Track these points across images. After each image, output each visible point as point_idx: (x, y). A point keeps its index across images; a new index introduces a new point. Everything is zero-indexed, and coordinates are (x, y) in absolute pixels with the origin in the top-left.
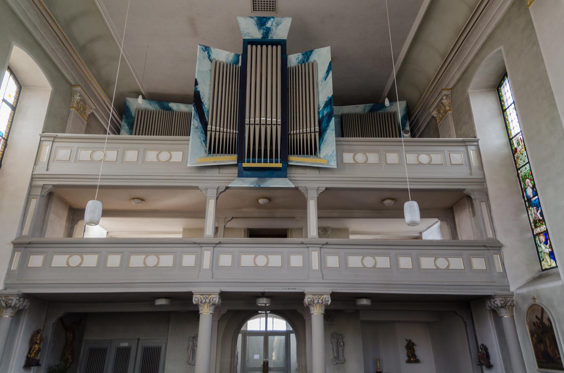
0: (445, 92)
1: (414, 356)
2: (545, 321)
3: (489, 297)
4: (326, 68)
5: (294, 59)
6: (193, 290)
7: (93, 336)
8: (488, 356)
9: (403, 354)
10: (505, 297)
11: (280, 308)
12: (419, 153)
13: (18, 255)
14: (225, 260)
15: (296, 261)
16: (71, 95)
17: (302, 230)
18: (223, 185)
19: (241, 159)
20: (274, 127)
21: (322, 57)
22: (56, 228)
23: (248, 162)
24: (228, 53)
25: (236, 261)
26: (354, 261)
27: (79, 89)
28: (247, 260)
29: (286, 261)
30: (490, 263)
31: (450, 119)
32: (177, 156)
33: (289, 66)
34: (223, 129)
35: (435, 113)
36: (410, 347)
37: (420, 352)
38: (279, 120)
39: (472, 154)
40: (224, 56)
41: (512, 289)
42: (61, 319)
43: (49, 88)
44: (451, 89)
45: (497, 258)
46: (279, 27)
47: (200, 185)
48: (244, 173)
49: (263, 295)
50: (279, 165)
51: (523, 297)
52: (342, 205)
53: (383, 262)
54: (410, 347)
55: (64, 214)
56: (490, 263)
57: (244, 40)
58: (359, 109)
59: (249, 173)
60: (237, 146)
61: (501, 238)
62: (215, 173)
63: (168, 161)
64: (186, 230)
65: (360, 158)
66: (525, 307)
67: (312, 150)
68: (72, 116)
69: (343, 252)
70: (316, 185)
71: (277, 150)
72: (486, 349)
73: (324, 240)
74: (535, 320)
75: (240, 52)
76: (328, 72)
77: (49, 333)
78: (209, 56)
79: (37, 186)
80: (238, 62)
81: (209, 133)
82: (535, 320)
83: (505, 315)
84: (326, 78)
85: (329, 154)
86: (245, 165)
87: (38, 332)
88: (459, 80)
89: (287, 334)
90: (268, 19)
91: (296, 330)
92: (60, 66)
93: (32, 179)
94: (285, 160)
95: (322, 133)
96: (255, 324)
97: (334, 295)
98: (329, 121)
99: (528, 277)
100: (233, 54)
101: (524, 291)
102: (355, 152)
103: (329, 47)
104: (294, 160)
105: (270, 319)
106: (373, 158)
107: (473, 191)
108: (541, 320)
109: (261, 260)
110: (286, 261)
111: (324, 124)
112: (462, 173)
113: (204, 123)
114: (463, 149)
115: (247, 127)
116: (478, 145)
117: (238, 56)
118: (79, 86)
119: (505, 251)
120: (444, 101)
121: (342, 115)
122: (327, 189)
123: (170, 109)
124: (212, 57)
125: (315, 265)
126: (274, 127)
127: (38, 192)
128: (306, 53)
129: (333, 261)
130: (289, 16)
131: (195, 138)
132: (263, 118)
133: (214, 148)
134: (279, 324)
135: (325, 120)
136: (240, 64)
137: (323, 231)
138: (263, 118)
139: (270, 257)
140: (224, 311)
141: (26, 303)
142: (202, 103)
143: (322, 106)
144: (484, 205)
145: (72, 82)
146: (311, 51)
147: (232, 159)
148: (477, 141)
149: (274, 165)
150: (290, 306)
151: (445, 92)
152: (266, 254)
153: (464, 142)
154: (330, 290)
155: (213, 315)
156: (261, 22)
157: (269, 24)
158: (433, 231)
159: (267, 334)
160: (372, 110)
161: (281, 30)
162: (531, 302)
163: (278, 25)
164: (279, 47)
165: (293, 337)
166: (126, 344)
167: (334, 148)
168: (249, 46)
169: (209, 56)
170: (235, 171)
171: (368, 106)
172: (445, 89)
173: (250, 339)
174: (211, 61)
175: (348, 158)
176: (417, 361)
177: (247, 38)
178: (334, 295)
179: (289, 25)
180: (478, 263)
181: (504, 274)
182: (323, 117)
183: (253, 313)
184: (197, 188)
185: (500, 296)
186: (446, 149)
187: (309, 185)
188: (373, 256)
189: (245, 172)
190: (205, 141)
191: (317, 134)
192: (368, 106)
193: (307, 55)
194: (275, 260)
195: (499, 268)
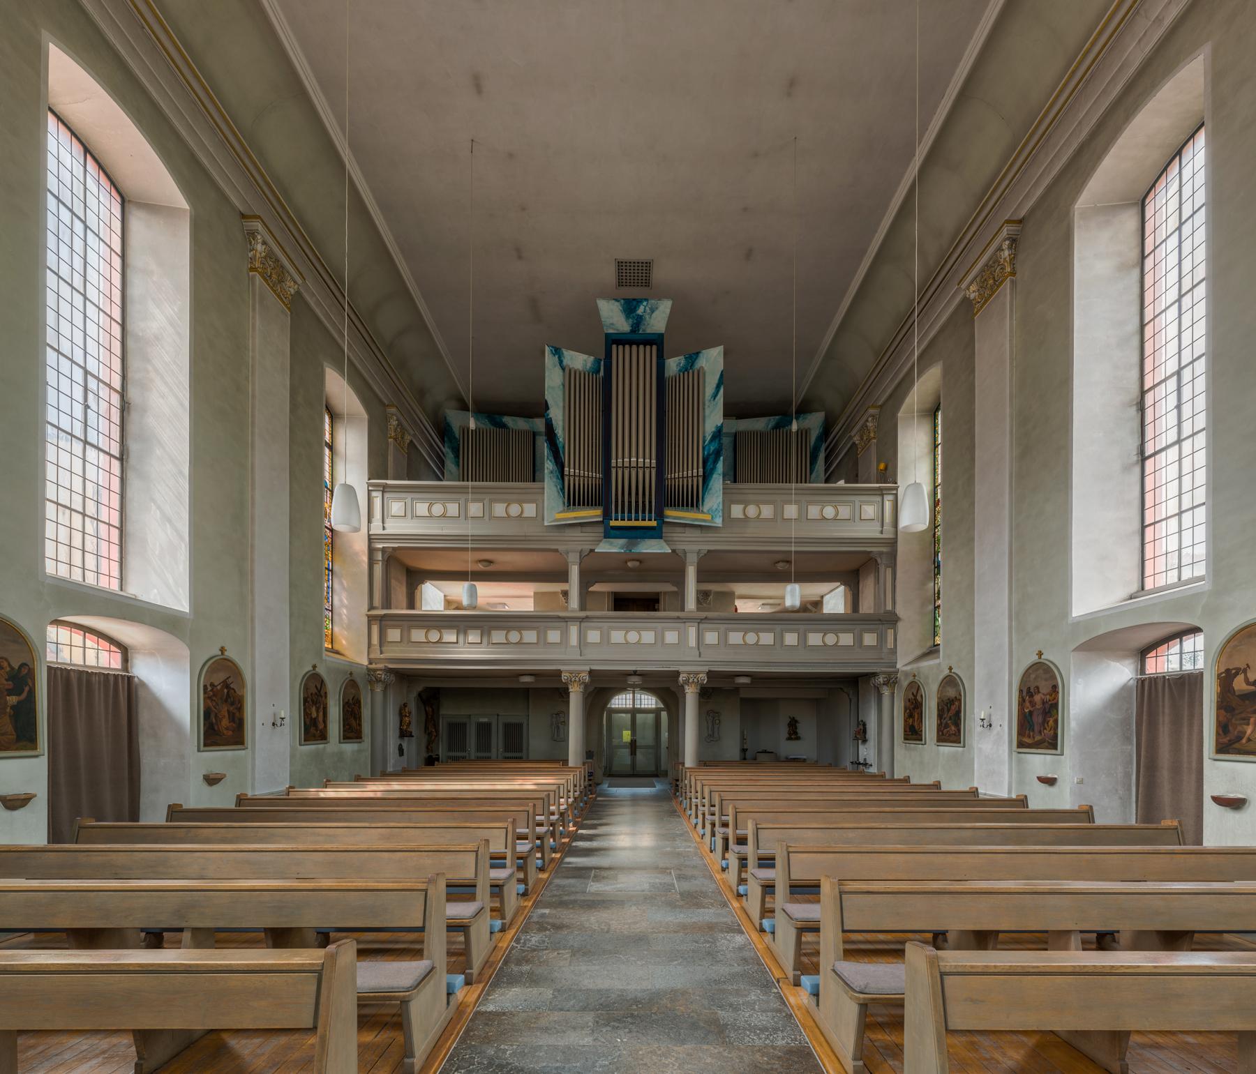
0: (871, 411)
1: (796, 733)
2: (919, 698)
3: (874, 675)
4: (716, 381)
5: (673, 365)
6: (562, 668)
7: (449, 711)
8: (865, 731)
9: (784, 731)
10: (889, 674)
11: (653, 686)
12: (823, 504)
13: (375, 629)
14: (594, 636)
15: (671, 637)
16: (386, 419)
17: (679, 597)
18: (587, 547)
19: (607, 515)
20: (647, 471)
21: (712, 361)
22: (400, 592)
23: (616, 519)
24: (585, 357)
25: (605, 638)
26: (735, 638)
27: (393, 410)
28: (617, 636)
29: (660, 638)
30: (882, 639)
31: (873, 450)
32: (530, 510)
33: (666, 375)
34: (583, 472)
35: (856, 439)
36: (793, 724)
37: (802, 730)
38: (654, 461)
39: (888, 506)
40: (579, 361)
41: (898, 666)
42: (420, 695)
43: (366, 416)
44: (881, 406)
45: (890, 632)
46: (654, 315)
47: (560, 548)
48: (611, 533)
49: (635, 673)
50: (654, 523)
51: (906, 674)
52: (723, 570)
53: (767, 638)
54: (793, 724)
55: (404, 579)
56: (882, 639)
57: (607, 335)
58: (760, 424)
59: (617, 532)
60: (599, 496)
61: (900, 611)
62: (576, 534)
63: (520, 516)
64: (538, 596)
65: (752, 511)
66: (905, 684)
67: (692, 501)
68: (391, 448)
69: (723, 627)
70: (696, 547)
71: (650, 502)
72: (864, 725)
73: (704, 614)
74: (911, 696)
75: (603, 357)
76: (718, 387)
77: (412, 706)
78: (561, 362)
79: (378, 549)
80: (598, 371)
81: (566, 479)
82: (911, 696)
83: (886, 692)
84: (715, 396)
85: (715, 507)
86: (613, 523)
87: (405, 705)
88: (891, 396)
89: (657, 712)
90: (639, 302)
91: (668, 707)
92: (370, 381)
93: (370, 539)
94: (660, 516)
95: (706, 478)
96: (621, 701)
97: (710, 674)
98: (716, 461)
99: (918, 652)
100: (592, 358)
101: (908, 668)
102: (746, 503)
103: (720, 349)
104: (672, 514)
105: (637, 696)
106: (767, 511)
107: (881, 553)
108: (915, 696)
109: (633, 637)
110: (660, 638)
111: (709, 465)
112: (870, 531)
113: (560, 465)
114: (879, 499)
115: (614, 471)
116: (896, 495)
117: (598, 361)
118: (393, 406)
119: (900, 625)
120: (870, 424)
121: (735, 435)
122: (709, 551)
123: (504, 426)
124: (565, 363)
125: (692, 642)
126: (647, 471)
127: (379, 556)
128: (690, 357)
129: (711, 637)
130: (667, 297)
131: (550, 486)
132: (634, 458)
133: (574, 499)
134: (648, 701)
135: (711, 460)
136: (602, 373)
137: (703, 596)
138: (634, 458)
139: (643, 633)
140: (591, 689)
141: (393, 678)
142: (555, 435)
143: (708, 438)
144: (889, 571)
145: (386, 402)
146: (698, 353)
147: (594, 514)
148: (896, 489)
149: (647, 523)
150: (666, 686)
151: (871, 411)
152: (638, 630)
153: (880, 489)
154: (706, 669)
155: (584, 693)
156: (630, 307)
157: (640, 311)
158: (835, 600)
159: (634, 712)
160: (778, 426)
161: (658, 319)
162: (911, 679)
163: (652, 311)
164: (654, 347)
165: (664, 715)
166: (485, 720)
167: (720, 499)
168: (614, 346)
169: (561, 362)
170: (601, 529)
171: (773, 420)
172: (873, 406)
173: (615, 716)
174: (563, 369)
175: (737, 511)
176: (798, 738)
177: (611, 331)
178: (710, 674)
179: (668, 311)
180: (870, 639)
181: (894, 651)
182: (709, 455)
183: (622, 689)
184: (556, 551)
185: (884, 673)
186: (857, 499)
187: (687, 547)
188: (757, 631)
189: (613, 532)
190: (563, 489)
191: (701, 479)
192: (773, 420)
193: (692, 358)
194: (648, 637)
195: (890, 645)
